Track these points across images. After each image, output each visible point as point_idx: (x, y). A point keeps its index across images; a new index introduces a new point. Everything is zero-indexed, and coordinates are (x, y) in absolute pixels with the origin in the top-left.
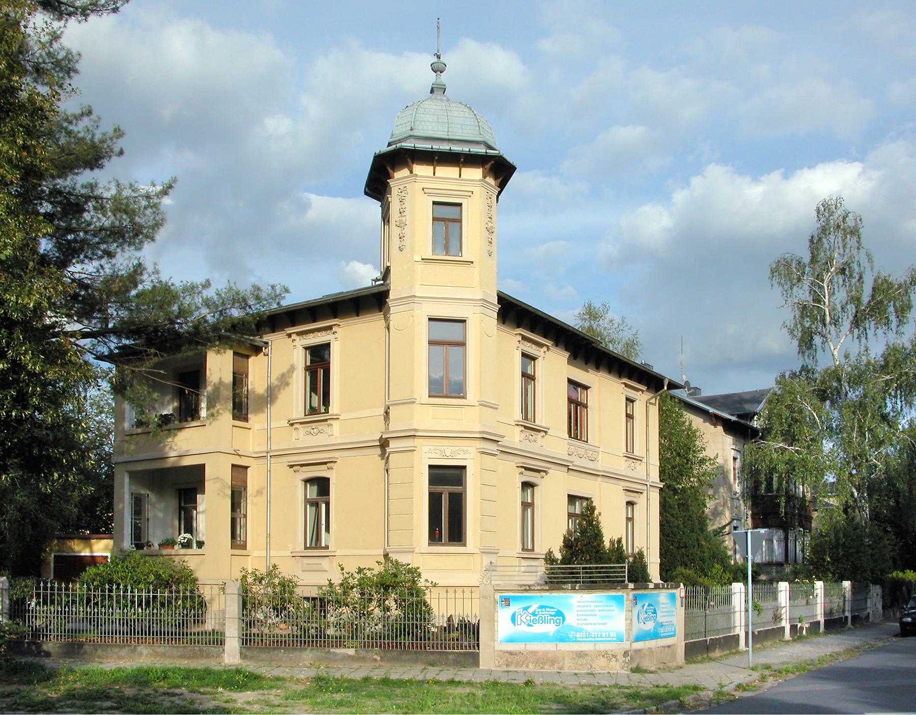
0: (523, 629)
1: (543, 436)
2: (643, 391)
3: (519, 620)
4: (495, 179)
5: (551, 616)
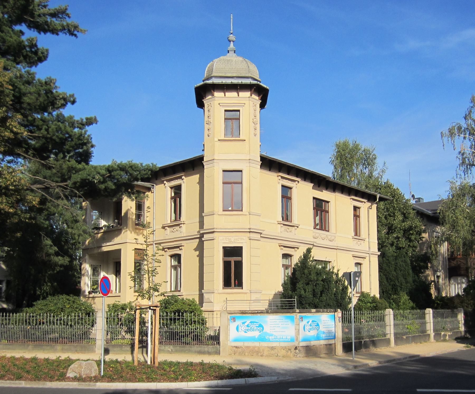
0: (242, 334)
1: (296, 229)
2: (365, 202)
3: (240, 329)
4: (259, 96)
5: (256, 327)
